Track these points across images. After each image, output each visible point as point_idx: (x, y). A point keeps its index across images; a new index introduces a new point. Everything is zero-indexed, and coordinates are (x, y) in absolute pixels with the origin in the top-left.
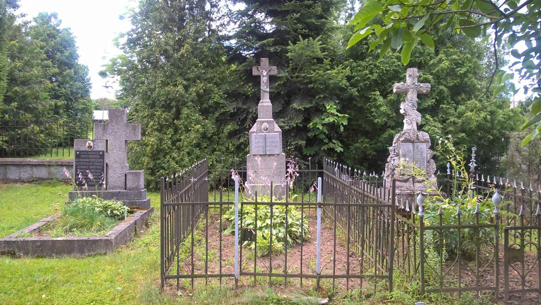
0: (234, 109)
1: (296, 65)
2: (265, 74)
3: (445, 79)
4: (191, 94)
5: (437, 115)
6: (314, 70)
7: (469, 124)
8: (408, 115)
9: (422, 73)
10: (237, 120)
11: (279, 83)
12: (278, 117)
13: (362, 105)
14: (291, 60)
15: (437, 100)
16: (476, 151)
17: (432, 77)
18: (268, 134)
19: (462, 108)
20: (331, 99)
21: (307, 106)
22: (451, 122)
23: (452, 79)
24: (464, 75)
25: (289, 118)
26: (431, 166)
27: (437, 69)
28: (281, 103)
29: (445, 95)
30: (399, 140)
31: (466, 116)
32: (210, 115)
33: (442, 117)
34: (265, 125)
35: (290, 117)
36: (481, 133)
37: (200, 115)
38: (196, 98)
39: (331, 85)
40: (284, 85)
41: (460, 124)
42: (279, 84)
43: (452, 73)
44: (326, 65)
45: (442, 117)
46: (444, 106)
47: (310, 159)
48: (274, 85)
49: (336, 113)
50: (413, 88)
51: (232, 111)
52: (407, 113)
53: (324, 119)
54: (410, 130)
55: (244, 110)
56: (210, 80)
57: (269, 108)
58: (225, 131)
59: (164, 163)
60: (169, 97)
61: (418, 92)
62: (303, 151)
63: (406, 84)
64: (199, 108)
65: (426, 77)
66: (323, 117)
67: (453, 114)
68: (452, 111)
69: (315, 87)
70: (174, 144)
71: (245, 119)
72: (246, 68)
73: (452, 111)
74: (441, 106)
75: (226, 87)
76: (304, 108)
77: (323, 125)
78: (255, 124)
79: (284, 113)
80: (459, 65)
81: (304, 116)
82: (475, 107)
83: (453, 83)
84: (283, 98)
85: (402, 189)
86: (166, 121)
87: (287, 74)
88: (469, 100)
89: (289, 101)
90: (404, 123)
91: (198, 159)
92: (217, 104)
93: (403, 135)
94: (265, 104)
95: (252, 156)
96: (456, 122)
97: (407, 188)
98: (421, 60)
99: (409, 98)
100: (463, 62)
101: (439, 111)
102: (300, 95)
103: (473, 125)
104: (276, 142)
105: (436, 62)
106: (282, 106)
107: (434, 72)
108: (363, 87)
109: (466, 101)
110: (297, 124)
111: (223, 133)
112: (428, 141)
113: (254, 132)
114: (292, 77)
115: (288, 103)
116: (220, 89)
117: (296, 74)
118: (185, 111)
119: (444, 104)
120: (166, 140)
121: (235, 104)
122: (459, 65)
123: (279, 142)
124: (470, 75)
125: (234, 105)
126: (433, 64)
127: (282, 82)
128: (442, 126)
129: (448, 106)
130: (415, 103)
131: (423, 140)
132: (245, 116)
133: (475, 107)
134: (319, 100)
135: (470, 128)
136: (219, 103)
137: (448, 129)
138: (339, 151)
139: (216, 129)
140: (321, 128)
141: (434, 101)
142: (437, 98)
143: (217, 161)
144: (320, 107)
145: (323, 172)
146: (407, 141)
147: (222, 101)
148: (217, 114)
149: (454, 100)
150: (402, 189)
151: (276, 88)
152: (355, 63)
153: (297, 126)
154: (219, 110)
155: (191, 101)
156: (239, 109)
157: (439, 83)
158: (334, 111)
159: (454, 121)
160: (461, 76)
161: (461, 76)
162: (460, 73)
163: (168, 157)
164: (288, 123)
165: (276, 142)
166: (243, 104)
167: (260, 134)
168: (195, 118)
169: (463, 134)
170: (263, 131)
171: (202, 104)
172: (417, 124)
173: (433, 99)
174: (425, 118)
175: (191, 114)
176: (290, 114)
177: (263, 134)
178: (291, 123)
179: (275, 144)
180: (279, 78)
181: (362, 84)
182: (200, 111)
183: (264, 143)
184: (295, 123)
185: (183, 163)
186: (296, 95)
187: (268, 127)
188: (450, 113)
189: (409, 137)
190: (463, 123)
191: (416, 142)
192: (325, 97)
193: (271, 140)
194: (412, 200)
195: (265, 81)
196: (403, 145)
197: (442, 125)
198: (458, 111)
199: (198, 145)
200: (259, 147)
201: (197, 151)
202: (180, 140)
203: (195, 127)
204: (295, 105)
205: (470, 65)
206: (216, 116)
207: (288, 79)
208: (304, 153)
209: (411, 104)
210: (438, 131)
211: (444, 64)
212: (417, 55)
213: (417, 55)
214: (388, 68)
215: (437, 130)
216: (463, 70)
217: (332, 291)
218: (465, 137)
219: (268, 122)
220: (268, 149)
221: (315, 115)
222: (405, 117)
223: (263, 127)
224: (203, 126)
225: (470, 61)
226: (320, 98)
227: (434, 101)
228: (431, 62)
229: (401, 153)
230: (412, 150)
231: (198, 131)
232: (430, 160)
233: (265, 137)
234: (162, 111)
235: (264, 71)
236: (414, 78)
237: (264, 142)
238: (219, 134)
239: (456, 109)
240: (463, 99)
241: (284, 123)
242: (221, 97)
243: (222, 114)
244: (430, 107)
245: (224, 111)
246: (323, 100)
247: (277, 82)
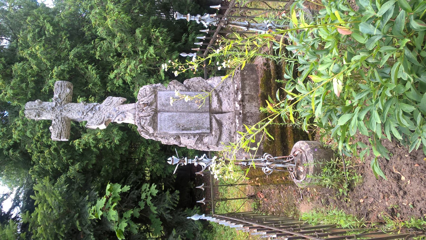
3: (62, 50)
5: (110, 63)
7: (123, 24)
8: (108, 117)
9: (50, 81)
13: (94, 156)
15: (89, 63)
16: (179, 12)
17: (56, 67)
19: (101, 32)
22: (119, 46)
23: (61, 41)
24: (56, 27)
26: (195, 85)
27: (45, 60)
29: (83, 51)
30: (153, 134)
31: (112, 26)
33: (113, 57)
36: (135, 9)
41: (123, 34)
43: (53, 42)
45: (113, 57)
46: (98, 53)
50: (61, 111)
52: (106, 119)
54: (134, 114)
61: (68, 102)
63: (53, 122)
65: (56, 76)
67: (109, 43)
68: (105, 44)
73: (105, 44)
74: (97, 58)
80: (41, 33)
82: (100, 14)
83: (67, 41)
85: (233, 131)
88: (91, 23)
90: (123, 124)
93: (143, 128)
96: (120, 40)
97: (232, 123)
98: (32, 81)
99: (79, 117)
100: (38, 26)
101: (105, 60)
103: (126, 18)
105: (35, 62)
107: (49, 64)
108: (69, 157)
109: (92, 25)
112: (154, 88)
119: (95, 54)
122: (42, 32)
124: (56, 19)
126: (37, 65)
128: (126, 59)
129: (98, 49)
130: (87, 107)
131: (153, 96)
133: (100, 14)
135: (129, 22)
137: (130, 50)
138: (157, 191)
141: (90, 67)
142: (86, 62)
146: (154, 123)
149: (91, 40)
150: (233, 131)
152: (35, 167)
157: (66, 58)
159: (119, 43)
160: (57, 30)
161: (57, 30)
162: (53, 31)
169: (138, 31)
172: (124, 103)
173: (87, 68)
174: (115, 78)
181: (64, 158)
188: (108, 47)
189: (148, 118)
190: (122, 31)
191: (156, 107)
194: (251, 117)
196: (161, 129)
197: (123, 57)
198: (105, 37)
205: (42, 18)
209: (89, 113)
210: (132, 64)
211: (37, 51)
212: (24, 85)
213: (24, 85)
214: (41, 126)
215: (132, 66)
216: (49, 27)
218: (141, 29)
222: (112, 121)
225: (37, 18)
227: (90, 67)
228: (35, 67)
229: (174, 132)
230: (170, 114)
232: (185, 86)
236: (43, 109)
239: (102, 39)
240: (89, 30)
244: (98, 72)
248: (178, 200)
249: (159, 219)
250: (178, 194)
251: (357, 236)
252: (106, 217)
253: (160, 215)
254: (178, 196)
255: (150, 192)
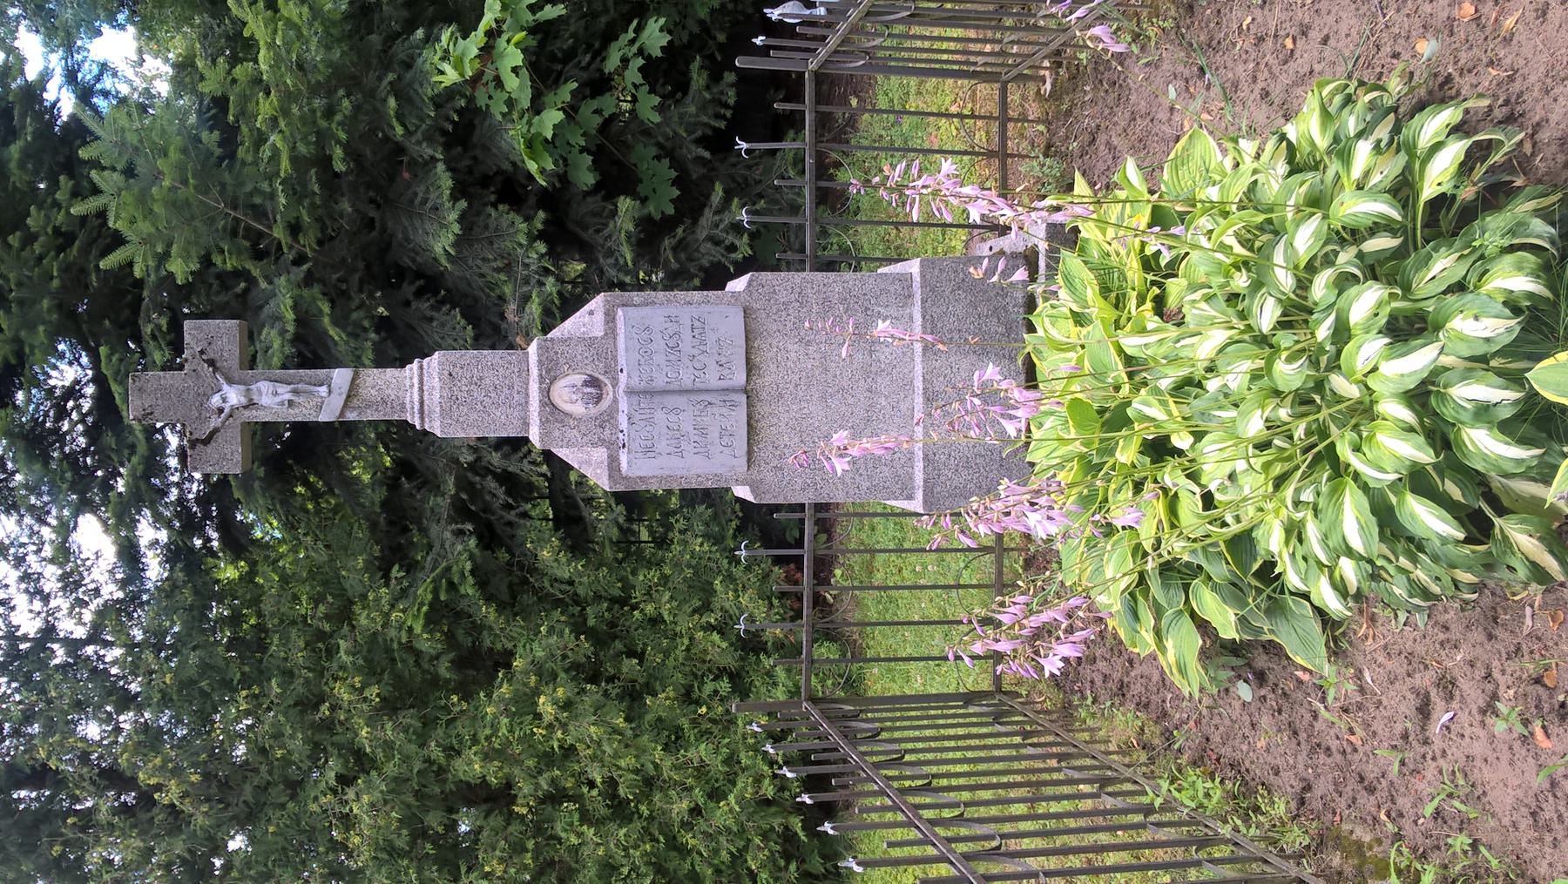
0: (460, 533)
1: (234, 233)
2: (234, 396)
4: (388, 746)
6: (260, 139)
10: (511, 516)
11: (326, 320)
12: (496, 329)
14: (206, 261)
18: (623, 378)
20: (408, 65)
21: (446, 182)
25: (503, 277)
28: (429, 313)
32: (487, 643)
34: (566, 394)
35: (498, 270)
37: (489, 696)
38: (409, 718)
39: (336, 54)
40: (337, 297)
42: (335, 323)
44: (234, 81)
47: (744, 145)
48: (342, 347)
49: (478, 38)
51: (472, 542)
53: (511, 103)
55: (463, 484)
56: (321, 645)
57: (457, 371)
58: (564, 572)
59: (716, 852)
60: (401, 843)
62: (658, 217)
64: (455, 698)
66: (498, 109)
69: (343, 136)
70: (620, 810)
71: (506, 479)
72: (257, 485)
75: (355, 569)
76: (454, 198)
77: (537, 107)
78: (554, 451)
79: (476, 300)
81: (495, 205)
84: (407, 304)
86: (518, 848)
87: (282, 281)
89: (419, 275)
91: (695, 696)
92: (437, 614)
94: (434, 398)
95: (754, 470)
102: (390, 224)
104: (672, 328)
106: (445, 309)
110: (532, 238)
111: (571, 583)
113: (613, 463)
114: (300, 260)
115: (431, 283)
116: (364, 597)
117: (279, 233)
118: (471, 766)
120: (607, 850)
121: (434, 530)
123: (672, 310)
125: (442, 533)
127: (326, 308)
132: (491, 484)
134: (412, 121)
136: (435, 604)
138: (664, 40)
139: (556, 614)
140: (552, 118)
143: (706, 607)
144: (448, 119)
145: (819, 77)
147: (424, 592)
148: (487, 613)
151: (354, 335)
153: (542, 236)
154: (463, 604)
155: (422, 745)
156: (461, 511)
158: (472, 46)
163: (690, 840)
164: (526, 281)
165: (672, 328)
166: (437, 489)
167: (624, 424)
168: (506, 720)
170: (605, 404)
171: (435, 682)
175: (488, 738)
176: (485, 269)
177: (623, 405)
178: (527, 266)
179: (687, 335)
180: (305, 320)
182: (467, 696)
183: (681, 401)
184: (530, 246)
185: (717, 765)
186: (389, 245)
187: (578, 379)
192: (398, 91)
193: (660, 358)
195: (285, 392)
199: (633, 696)
200: (702, 431)
201: (661, 703)
202: (612, 783)
203: (547, 718)
204: (441, 242)
206: (492, 616)
207: (309, 280)
208: (670, 210)
217: (1115, 141)
219: (549, 377)
220: (712, 378)
221: (486, 148)
223: (578, 409)
224: (547, 677)
226: (400, 117)
231: (567, 705)
233: (644, 393)
234: (469, 870)
235: (216, 400)
237: (671, 401)
238: (577, 600)
241: (526, 299)
242: (404, 593)
243: (482, 584)
245: (471, 580)
246: (410, 101)
247: (326, 333)
248: (731, 102)
249: (666, 162)
250: (732, 85)
251: (1048, 874)
252: (488, 106)
253: (668, 145)
254: (732, 93)
255: (637, 45)
